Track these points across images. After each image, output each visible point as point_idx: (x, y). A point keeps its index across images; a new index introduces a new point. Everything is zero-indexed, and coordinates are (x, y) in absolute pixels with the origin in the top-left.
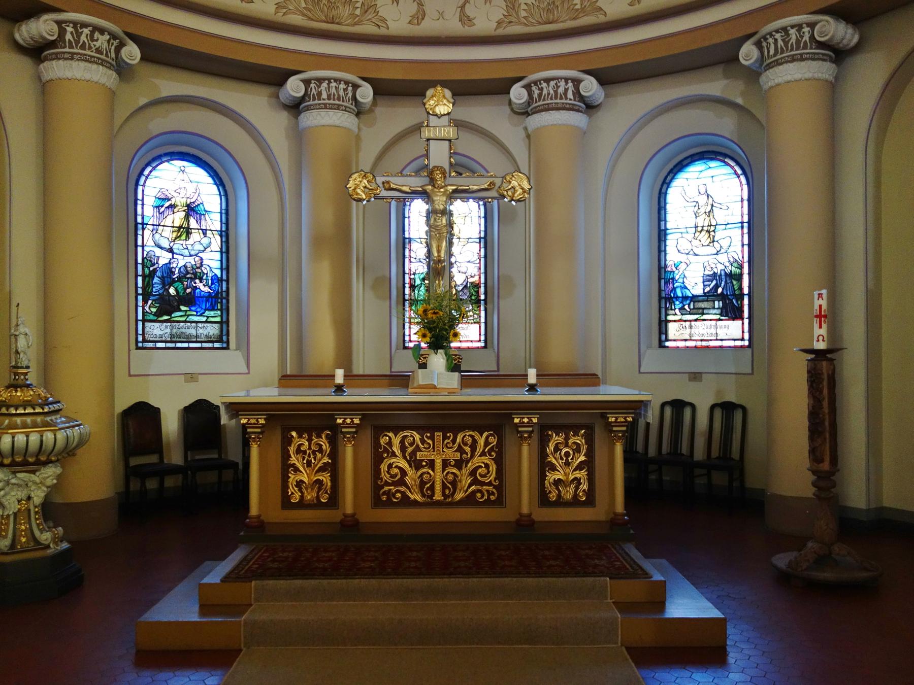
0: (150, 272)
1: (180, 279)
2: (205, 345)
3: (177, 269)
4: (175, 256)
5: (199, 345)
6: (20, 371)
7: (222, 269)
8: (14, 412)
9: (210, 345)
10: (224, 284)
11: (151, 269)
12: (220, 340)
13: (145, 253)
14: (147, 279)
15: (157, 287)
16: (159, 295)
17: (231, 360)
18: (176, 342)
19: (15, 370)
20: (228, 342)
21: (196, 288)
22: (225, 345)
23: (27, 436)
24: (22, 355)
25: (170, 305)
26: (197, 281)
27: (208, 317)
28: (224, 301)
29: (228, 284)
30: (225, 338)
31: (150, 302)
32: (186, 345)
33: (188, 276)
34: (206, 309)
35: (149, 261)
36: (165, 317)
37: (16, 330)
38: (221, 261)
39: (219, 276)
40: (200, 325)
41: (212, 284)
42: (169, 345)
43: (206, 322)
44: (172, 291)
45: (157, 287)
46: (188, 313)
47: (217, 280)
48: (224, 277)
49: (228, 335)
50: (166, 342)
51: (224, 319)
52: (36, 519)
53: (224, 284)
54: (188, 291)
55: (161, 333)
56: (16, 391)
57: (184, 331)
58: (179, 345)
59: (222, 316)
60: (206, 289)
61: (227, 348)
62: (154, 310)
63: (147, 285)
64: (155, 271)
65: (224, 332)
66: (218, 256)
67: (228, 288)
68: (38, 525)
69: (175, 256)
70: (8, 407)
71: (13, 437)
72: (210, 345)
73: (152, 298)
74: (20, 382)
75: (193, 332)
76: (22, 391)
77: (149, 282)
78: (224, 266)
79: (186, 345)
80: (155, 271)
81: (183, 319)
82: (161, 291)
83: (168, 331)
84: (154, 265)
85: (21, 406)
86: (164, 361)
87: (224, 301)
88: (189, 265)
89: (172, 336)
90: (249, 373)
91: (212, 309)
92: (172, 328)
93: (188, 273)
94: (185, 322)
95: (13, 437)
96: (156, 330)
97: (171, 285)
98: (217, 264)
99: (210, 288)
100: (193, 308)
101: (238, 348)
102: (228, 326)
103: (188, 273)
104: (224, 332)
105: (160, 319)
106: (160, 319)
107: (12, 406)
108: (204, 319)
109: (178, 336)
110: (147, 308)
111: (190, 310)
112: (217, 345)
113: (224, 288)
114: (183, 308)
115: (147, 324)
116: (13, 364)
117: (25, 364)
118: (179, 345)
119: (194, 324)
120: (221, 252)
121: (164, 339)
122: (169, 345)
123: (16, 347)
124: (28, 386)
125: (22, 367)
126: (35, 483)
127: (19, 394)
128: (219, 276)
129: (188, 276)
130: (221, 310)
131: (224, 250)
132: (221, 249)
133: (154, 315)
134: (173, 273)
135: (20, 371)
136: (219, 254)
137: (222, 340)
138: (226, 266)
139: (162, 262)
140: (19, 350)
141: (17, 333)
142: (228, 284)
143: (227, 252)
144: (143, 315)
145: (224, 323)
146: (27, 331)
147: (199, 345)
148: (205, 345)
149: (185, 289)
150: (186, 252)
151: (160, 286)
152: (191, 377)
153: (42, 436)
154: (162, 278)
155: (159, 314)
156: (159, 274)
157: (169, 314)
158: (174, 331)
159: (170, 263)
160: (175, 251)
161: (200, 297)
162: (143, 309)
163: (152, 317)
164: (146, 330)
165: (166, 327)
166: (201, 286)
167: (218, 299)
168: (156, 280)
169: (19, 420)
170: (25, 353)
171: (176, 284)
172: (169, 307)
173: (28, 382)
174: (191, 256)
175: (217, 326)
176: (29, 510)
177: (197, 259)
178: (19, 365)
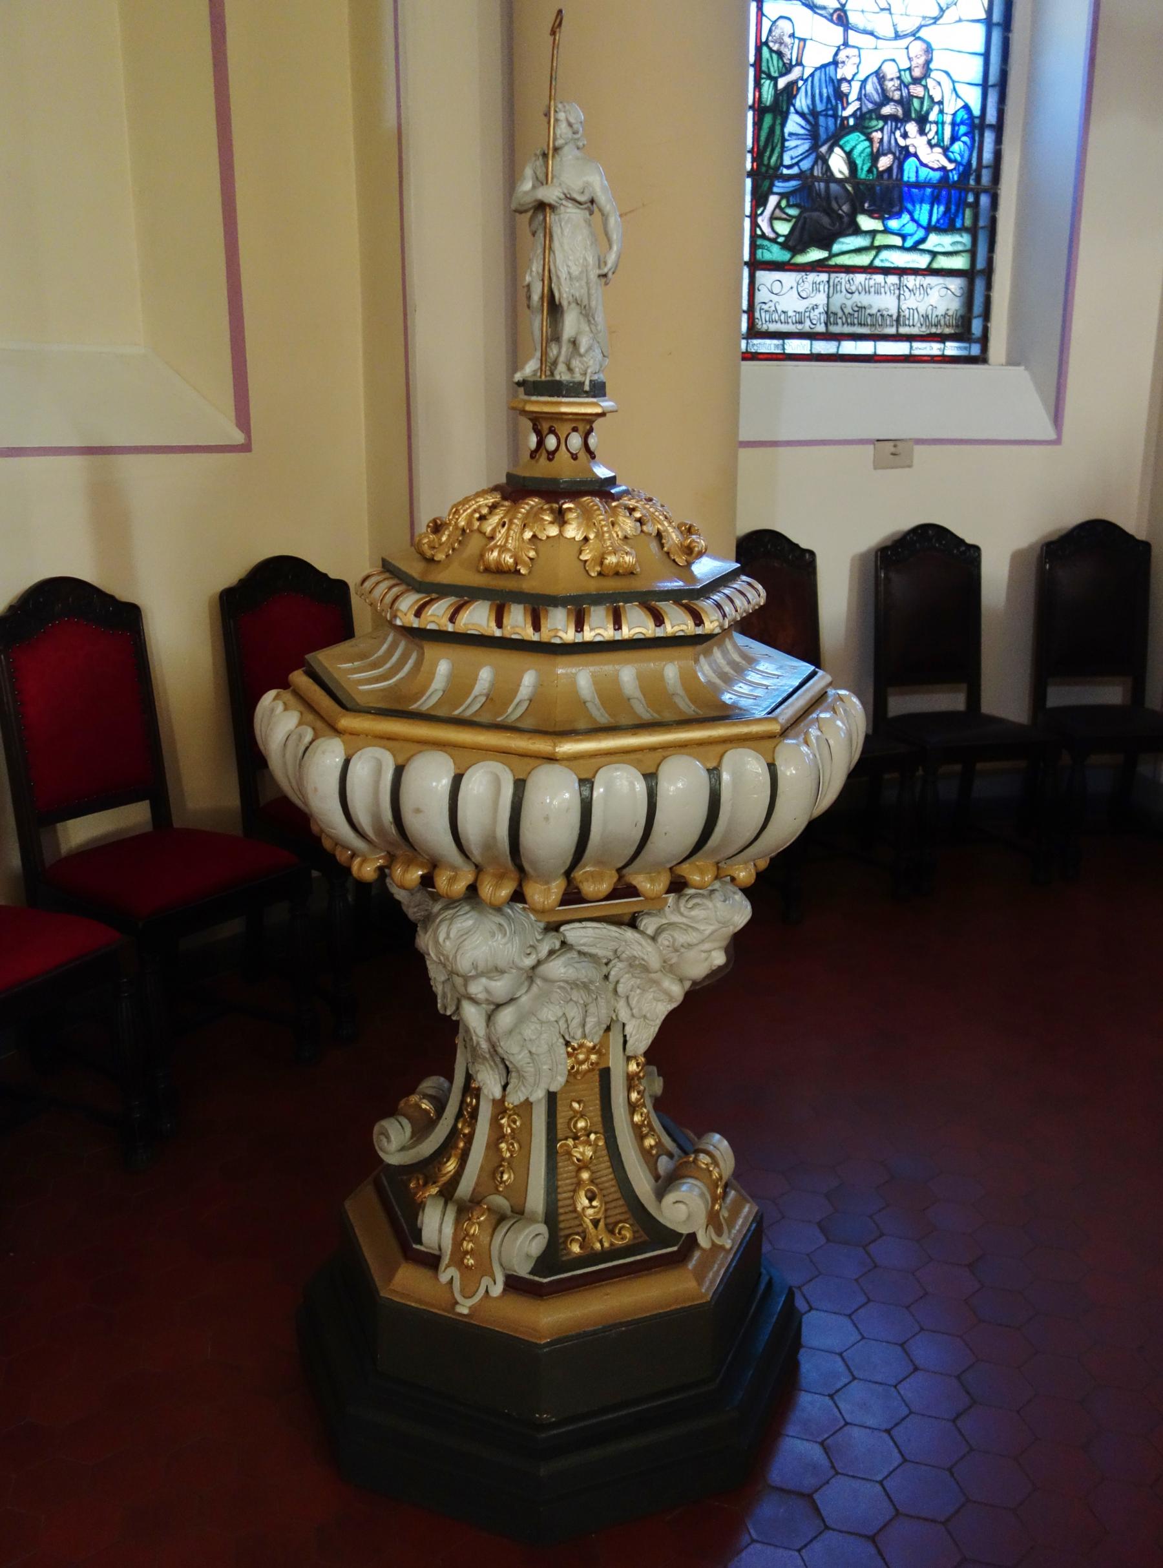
0: (778, 94)
1: (862, 123)
2: (921, 349)
3: (856, 86)
4: (854, 38)
5: (901, 348)
6: (570, 406)
7: (985, 86)
8: (569, 635)
9: (934, 349)
10: (989, 137)
11: (782, 83)
12: (962, 333)
13: (766, 25)
14: (768, 120)
15: (795, 150)
16: (799, 176)
17: (1000, 394)
18: (839, 337)
19: (541, 404)
20: (984, 340)
21: (905, 153)
22: (975, 350)
23: (651, 778)
24: (571, 323)
25: (829, 212)
26: (912, 128)
27: (934, 254)
28: (984, 200)
29: (999, 141)
30: (976, 327)
31: (773, 200)
32: (865, 348)
33: (887, 110)
34: (930, 229)
35: (771, 61)
36: (815, 255)
37: (542, 180)
38: (986, 56)
39: (976, 111)
40: (910, 281)
41: (954, 138)
42: (822, 347)
43: (930, 271)
44: (838, 164)
45: (795, 150)
46: (880, 240)
47: (975, 126)
48: (991, 117)
49: (986, 315)
50: (812, 336)
51: (981, 264)
52: (633, 1108)
53: (989, 137)
54: (884, 162)
55: (801, 306)
56: (560, 518)
57: (864, 299)
58: (848, 347)
59: (973, 253)
60: (935, 158)
61: (981, 359)
62: (784, 228)
63: (768, 145)
64: (790, 92)
65: (978, 308)
66: (976, 37)
67: (998, 155)
68: (639, 1133)
69: (854, 38)
70: (538, 606)
71: (587, 782)
72: (934, 349)
73: (779, 187)
74: (564, 469)
75: (886, 302)
76: (587, 516)
77: (772, 130)
78: (993, 78)
79: (865, 348)
80: (790, 92)
81: (863, 260)
82: (806, 165)
83: (820, 299)
84: (787, 69)
85: (597, 599)
86: (806, 400)
87: (984, 200)
88: (890, 71)
89: (830, 315)
90: (1057, 441)
91: (947, 226)
92: (832, 289)
93: (886, 100)
94: (870, 269)
95: (587, 782)
96: (789, 296)
97: (835, 140)
98: (974, 69)
99: (946, 151)
100: (893, 224)
101: (1012, 362)
102: (989, 286)
103: (886, 100)
104: (978, 308)
105: (801, 259)
106: (801, 259)
107: (555, 601)
108: (922, 261)
109: (849, 319)
110: (763, 222)
111: (887, 231)
112: (952, 349)
113: (988, 156)
114: (866, 222)
115: (763, 276)
116: (529, 369)
117: (587, 368)
118: (848, 347)
119: (893, 279)
120: (989, 23)
121: (806, 327)
122: (822, 347)
123: (548, 277)
124: (603, 490)
125: (575, 389)
126: (638, 967)
127: (573, 531)
128: (976, 111)
129: (887, 110)
130: (973, 231)
131: (997, 17)
132: (989, 12)
133: (784, 246)
134: (841, 97)
135: (570, 406)
136: (981, 29)
137: (968, 330)
138: (997, 84)
139: (815, 57)
140: (565, 292)
141: (550, 194)
142: (999, 141)
143: (1007, 24)
144: (754, 247)
145: (977, 276)
146: (596, 181)
147: (901, 348)
148: (921, 349)
149: (874, 158)
150: (883, 25)
151: (806, 146)
152: (893, 452)
153: (714, 773)
154: (811, 117)
155: (796, 243)
156: (802, 102)
157: (826, 243)
158: (838, 300)
159: (835, 63)
160: (853, 18)
161: (918, 185)
162: (755, 225)
163: (776, 253)
164: (761, 296)
165: (816, 287)
166: (917, 142)
167: (966, 198)
168: (794, 124)
169: (583, 677)
170: (587, 313)
171: (855, 140)
172: (825, 220)
173: (602, 472)
174: (897, 36)
175: (956, 285)
176: (605, 1075)
177: (917, 48)
178: (562, 374)
